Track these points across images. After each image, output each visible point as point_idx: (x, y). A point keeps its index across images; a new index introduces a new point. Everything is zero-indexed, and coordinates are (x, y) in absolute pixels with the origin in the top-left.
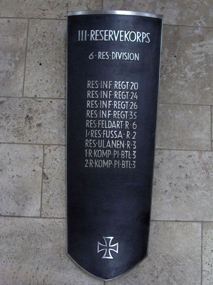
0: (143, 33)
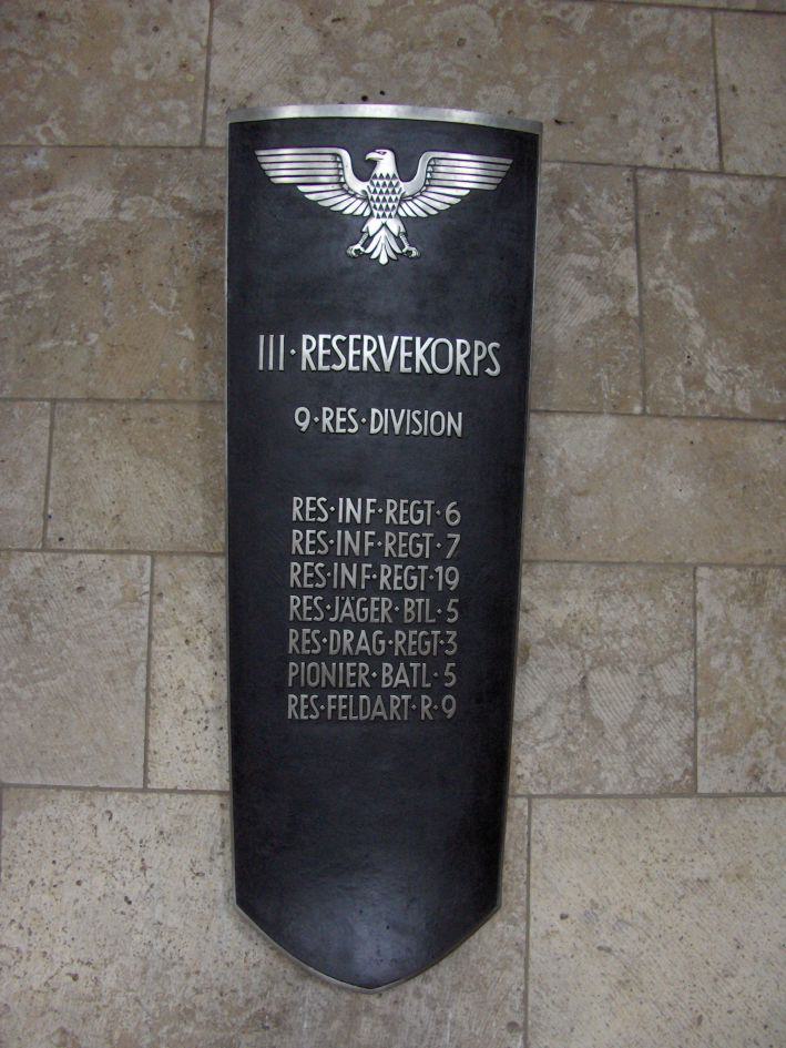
0: (477, 343)
